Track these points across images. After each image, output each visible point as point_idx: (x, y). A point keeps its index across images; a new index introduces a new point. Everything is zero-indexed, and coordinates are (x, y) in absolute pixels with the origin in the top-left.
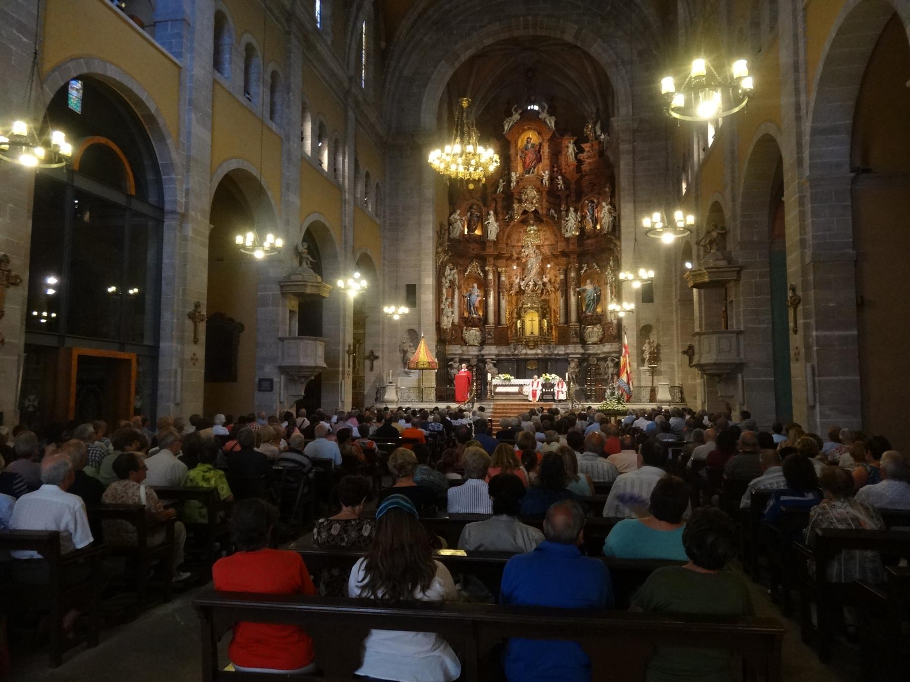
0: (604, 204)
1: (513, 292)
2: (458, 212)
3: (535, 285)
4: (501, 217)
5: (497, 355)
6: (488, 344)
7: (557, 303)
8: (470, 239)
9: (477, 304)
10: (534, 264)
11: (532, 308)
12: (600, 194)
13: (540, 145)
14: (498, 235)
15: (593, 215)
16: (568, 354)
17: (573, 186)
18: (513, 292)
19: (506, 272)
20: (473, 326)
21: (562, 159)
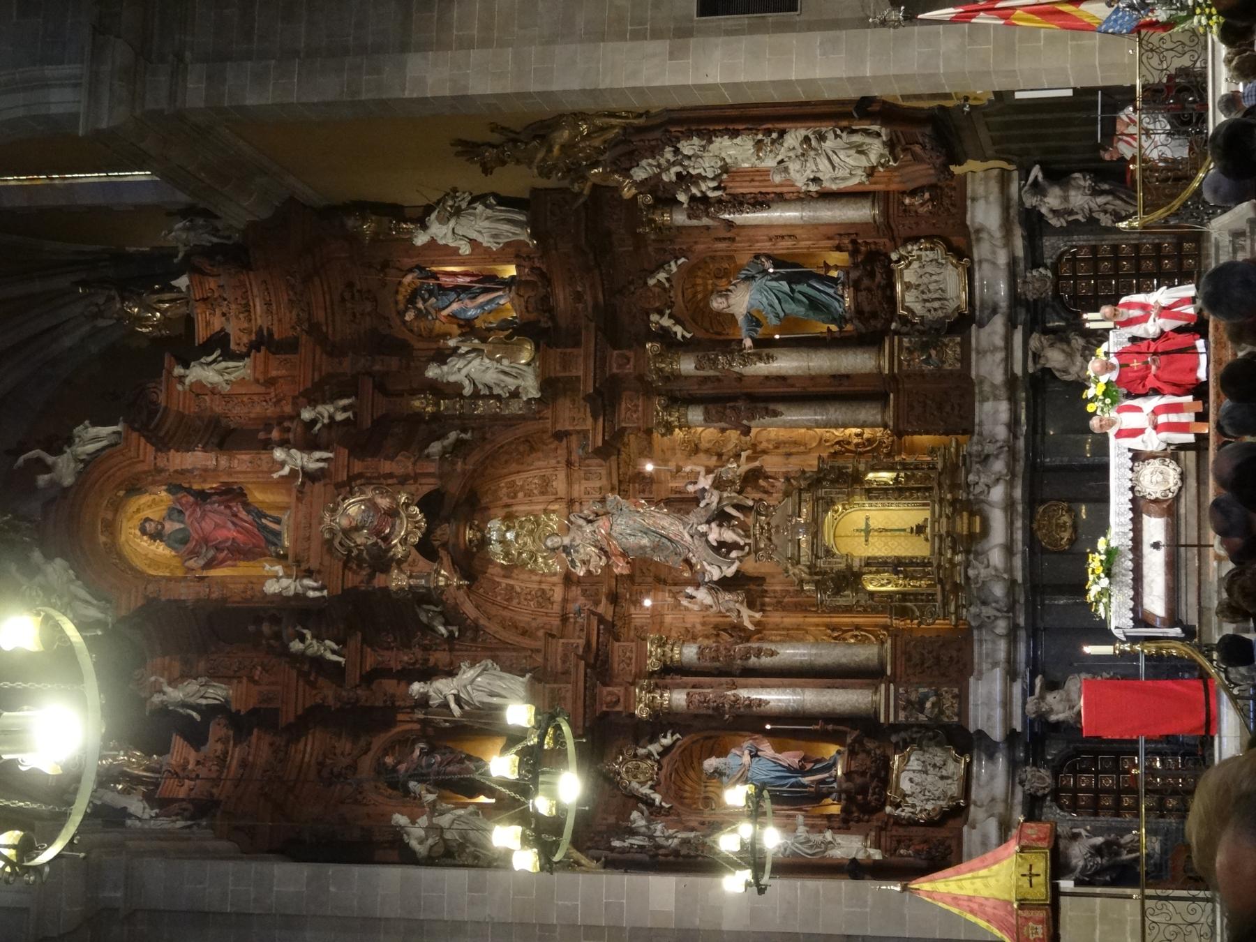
0: (421, 239)
1: (748, 618)
2: (401, 819)
3: (721, 517)
4: (440, 657)
5: (1011, 674)
6: (963, 712)
7: (801, 432)
9: (790, 758)
10: (634, 526)
11: (815, 528)
13: (174, 489)
15: (460, 290)
16: (1011, 382)
17: (346, 366)
18: (748, 618)
19: (662, 643)
20: (883, 775)
21: (239, 414)
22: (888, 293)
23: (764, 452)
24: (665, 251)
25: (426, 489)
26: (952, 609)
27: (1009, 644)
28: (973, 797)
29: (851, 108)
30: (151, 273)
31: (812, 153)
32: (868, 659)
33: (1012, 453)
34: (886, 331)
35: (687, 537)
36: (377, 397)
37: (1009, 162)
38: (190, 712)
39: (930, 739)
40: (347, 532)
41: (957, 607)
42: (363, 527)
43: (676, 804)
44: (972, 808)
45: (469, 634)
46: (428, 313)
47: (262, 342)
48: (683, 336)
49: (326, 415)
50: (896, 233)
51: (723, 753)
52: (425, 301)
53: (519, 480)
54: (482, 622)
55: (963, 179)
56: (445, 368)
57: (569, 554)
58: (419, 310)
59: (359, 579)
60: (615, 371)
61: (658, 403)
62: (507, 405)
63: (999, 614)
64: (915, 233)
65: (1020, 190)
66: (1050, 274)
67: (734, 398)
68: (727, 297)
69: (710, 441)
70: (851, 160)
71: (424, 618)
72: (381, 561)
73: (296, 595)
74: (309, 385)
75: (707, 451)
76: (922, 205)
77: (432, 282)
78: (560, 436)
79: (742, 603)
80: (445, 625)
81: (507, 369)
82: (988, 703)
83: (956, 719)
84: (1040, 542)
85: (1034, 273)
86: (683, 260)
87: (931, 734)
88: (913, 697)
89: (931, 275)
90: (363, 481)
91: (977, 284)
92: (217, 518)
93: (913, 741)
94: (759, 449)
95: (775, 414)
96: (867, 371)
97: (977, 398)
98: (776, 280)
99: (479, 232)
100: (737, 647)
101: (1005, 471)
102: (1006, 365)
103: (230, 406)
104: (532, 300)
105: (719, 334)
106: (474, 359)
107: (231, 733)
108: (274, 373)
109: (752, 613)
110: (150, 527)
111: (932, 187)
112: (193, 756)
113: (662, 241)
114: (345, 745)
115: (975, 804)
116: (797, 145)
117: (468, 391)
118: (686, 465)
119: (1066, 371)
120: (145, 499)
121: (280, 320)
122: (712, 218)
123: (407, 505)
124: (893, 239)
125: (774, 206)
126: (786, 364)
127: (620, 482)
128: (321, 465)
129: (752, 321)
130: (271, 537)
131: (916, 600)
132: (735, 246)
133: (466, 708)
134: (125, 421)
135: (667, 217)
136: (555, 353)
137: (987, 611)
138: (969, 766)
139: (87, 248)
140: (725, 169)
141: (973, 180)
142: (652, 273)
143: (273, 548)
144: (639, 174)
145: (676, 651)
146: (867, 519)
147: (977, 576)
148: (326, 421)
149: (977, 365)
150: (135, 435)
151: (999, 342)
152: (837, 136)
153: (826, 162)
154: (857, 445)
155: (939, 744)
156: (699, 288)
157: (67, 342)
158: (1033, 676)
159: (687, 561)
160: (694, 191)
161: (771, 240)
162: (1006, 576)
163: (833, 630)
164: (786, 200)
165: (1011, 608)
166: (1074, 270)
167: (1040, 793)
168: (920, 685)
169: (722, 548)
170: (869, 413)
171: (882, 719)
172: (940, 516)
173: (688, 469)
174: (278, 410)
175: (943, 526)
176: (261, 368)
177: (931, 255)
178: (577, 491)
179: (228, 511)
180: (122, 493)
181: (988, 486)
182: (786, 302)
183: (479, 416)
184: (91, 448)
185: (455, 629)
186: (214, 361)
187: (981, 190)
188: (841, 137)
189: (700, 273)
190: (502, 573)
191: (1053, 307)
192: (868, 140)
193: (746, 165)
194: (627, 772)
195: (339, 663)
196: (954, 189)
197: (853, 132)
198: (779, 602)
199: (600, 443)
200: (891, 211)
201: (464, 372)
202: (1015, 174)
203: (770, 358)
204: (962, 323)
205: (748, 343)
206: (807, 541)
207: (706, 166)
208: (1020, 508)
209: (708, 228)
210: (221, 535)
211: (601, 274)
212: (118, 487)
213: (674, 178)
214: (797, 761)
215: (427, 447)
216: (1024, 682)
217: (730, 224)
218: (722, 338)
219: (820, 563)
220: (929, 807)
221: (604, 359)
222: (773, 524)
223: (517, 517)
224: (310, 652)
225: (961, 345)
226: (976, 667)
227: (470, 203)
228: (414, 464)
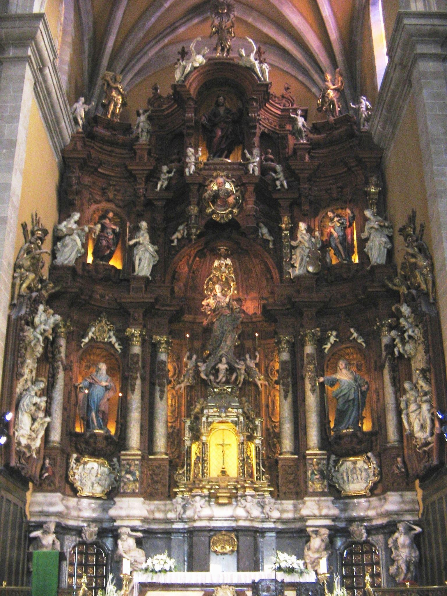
2: (77, 216)
5: (145, 520)
6: (125, 494)
16: (303, 519)
27: (164, 519)
35: (221, 353)
41: (182, 491)
44: (76, 500)
48: (325, 348)
49: (279, 176)
52: (338, 221)
58: (334, 218)
63: (178, 513)
65: (408, 521)
68: (346, 368)
71: (181, 228)
74: (293, 167)
76: (397, 467)
77: (348, 224)
83: (122, 491)
85: (364, 531)
86: (364, 345)
89: (361, 475)
95: (286, 397)
102: (312, 516)
105: (327, 367)
109: (183, 388)
115: (79, 501)
119: (309, 549)
126: (311, 400)
128: (251, 172)
129: (333, 381)
137: (180, 509)
142: (357, 330)
149: (312, 501)
156: (351, 357)
158: (143, 531)
161: (376, 389)
166: (367, 552)
167: (83, 535)
168: (142, 472)
171: (123, 452)
199: (268, 308)
202: (416, 518)
205: (322, 379)
214: (103, 409)
217: (382, 367)
218: (325, 368)
220: (77, 477)
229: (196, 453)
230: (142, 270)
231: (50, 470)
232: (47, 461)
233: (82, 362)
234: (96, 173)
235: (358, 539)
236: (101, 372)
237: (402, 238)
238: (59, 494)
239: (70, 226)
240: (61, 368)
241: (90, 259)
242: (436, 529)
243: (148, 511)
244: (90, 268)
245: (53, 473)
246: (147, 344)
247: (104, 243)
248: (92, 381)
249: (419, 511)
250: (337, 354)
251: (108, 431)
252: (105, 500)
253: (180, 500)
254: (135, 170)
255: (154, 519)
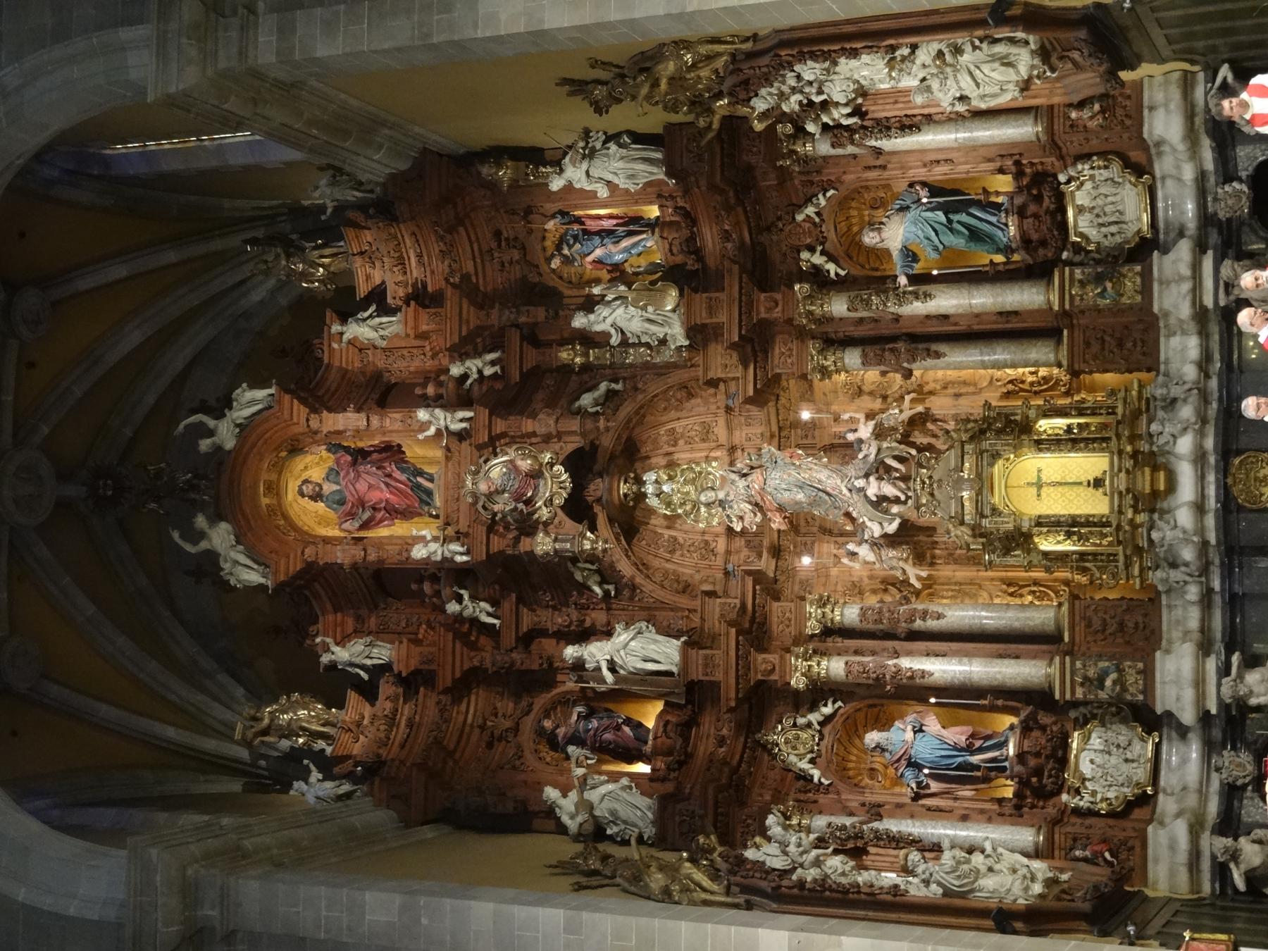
0: (556, 184)
1: (914, 574)
2: (551, 793)
3: (880, 470)
4: (598, 617)
5: (1205, 648)
6: (1149, 689)
8: (675, 752)
9: (957, 735)
10: (792, 479)
11: (982, 484)
12: (525, 204)
13: (334, 448)
14: (668, 632)
15: (605, 234)
17: (497, 317)
19: (822, 603)
20: (1060, 756)
21: (403, 367)
22: (1059, 218)
23: (931, 393)
24: (812, 183)
25: (570, 448)
26: (1136, 571)
27: (1203, 611)
28: (1162, 783)
29: (984, 14)
30: (326, 228)
31: (948, 70)
32: (1043, 624)
33: (1204, 396)
34: (1056, 262)
35: (845, 491)
36: (525, 352)
37: (1192, 62)
38: (358, 670)
39: (1113, 715)
40: (490, 496)
41: (1142, 570)
42: (504, 491)
43: (837, 782)
44: (1161, 797)
45: (626, 593)
46: (574, 259)
47: (421, 297)
48: (837, 274)
49: (474, 370)
50: (1064, 150)
51: (885, 725)
52: (570, 247)
53: (678, 426)
54: (639, 580)
55: (1138, 86)
56: (592, 317)
57: (724, 509)
58: (565, 256)
59: (506, 542)
60: (763, 315)
61: (812, 347)
62: (658, 352)
63: (1188, 578)
64: (1086, 150)
65: (1206, 93)
66: (1245, 189)
67: (894, 339)
68: (879, 230)
69: (874, 383)
70: (997, 74)
71: (578, 577)
72: (528, 526)
73: (444, 559)
75: (871, 393)
76: (1091, 118)
77: (576, 227)
78: (713, 383)
79: (906, 560)
80: (600, 584)
81: (652, 317)
82: (1177, 682)
83: (1141, 697)
84: (1236, 499)
85: (1227, 188)
86: (831, 192)
87: (1114, 709)
88: (1091, 673)
89: (1106, 196)
90: (507, 440)
91: (1160, 205)
92: (372, 481)
93: (1094, 717)
94: (926, 389)
95: (938, 355)
96: (1036, 307)
97: (1163, 332)
98: (932, 210)
99: (615, 174)
100: (902, 609)
101: (1193, 420)
103: (390, 361)
104: (676, 242)
105: (877, 270)
106: (619, 306)
107: (400, 690)
108: (424, 328)
110: (307, 489)
111: (1103, 97)
112: (367, 710)
113: (808, 173)
114: (507, 706)
115: (1165, 791)
116: (928, 61)
117: (615, 340)
118: (845, 412)
120: (309, 459)
121: (433, 272)
122: (858, 146)
123: (552, 465)
124: (1061, 157)
125: (924, 128)
126: (947, 301)
127: (780, 429)
128: (464, 425)
129: (908, 256)
130: (425, 497)
131: (1095, 560)
132: (886, 174)
133: (622, 672)
134: (277, 384)
135: (809, 147)
136: (700, 299)
137: (1176, 575)
138: (1158, 747)
139: (266, 204)
140: (862, 92)
141: (1151, 86)
143: (426, 509)
144: (760, 105)
145: (837, 612)
146: (1039, 471)
147: (1163, 539)
148: (475, 376)
149: (1160, 297)
150: (287, 397)
151: (1186, 271)
152: (975, 48)
153: (969, 79)
154: (1032, 384)
155: (1124, 721)
156: (854, 221)
157: (257, 296)
158: (1229, 652)
159: (848, 515)
160: (825, 119)
161: (925, 166)
162: (1195, 539)
163: (1009, 585)
164: (936, 122)
165: (1205, 570)
167: (1239, 783)
168: (1100, 657)
169: (881, 503)
170: (1040, 351)
171: (1057, 696)
172: (1120, 470)
173: (846, 416)
174: (436, 362)
175: (1122, 482)
176: (411, 323)
177: (1105, 174)
178: (739, 437)
179: (380, 473)
180: (284, 454)
181: (1173, 436)
182: (944, 233)
183: (631, 365)
184: (247, 412)
185: (611, 587)
186: (371, 316)
187: (1159, 97)
188: (980, 49)
189: (854, 204)
190: (665, 523)
191: (1250, 225)
192: (1014, 50)
193: (882, 86)
194: (786, 743)
195: (494, 625)
196: (1129, 97)
197: (996, 41)
198: (951, 555)
199: (751, 392)
200: (1056, 127)
201: (609, 321)
203: (927, 296)
204: (1144, 249)
205: (903, 280)
206: (970, 499)
207: (838, 91)
208: (1212, 459)
209: (855, 156)
210: (374, 497)
211: (746, 212)
212: (278, 449)
213: (797, 108)
214: (964, 738)
215: (578, 398)
216: (1218, 659)
217: (878, 152)
218: (878, 274)
219: (985, 522)
220: (1111, 795)
221: (750, 304)
222: (936, 478)
223: (679, 465)
224: (466, 613)
225: (1142, 275)
226: (1165, 636)
227: (605, 142)
228: (557, 421)
229: (1059, 542)
230: (667, 656)
231: (1097, 848)
232: (1078, 853)
233: (863, 784)
234: (458, 755)
235: (1244, 199)
236: (884, 743)
237: (615, 110)
238: (1150, 829)
239: (573, 809)
240: (876, 825)
241: (642, 768)
242: (1226, 32)
243: (1184, 642)
244: (660, 764)
245: (1104, 841)
246: (821, 646)
247: (608, 736)
248: (904, 762)
249: (1185, 72)
250: (852, 249)
251: (1012, 727)
252: (1161, 737)
253: (1159, 574)
254: (453, 673)
255: (1202, 631)
